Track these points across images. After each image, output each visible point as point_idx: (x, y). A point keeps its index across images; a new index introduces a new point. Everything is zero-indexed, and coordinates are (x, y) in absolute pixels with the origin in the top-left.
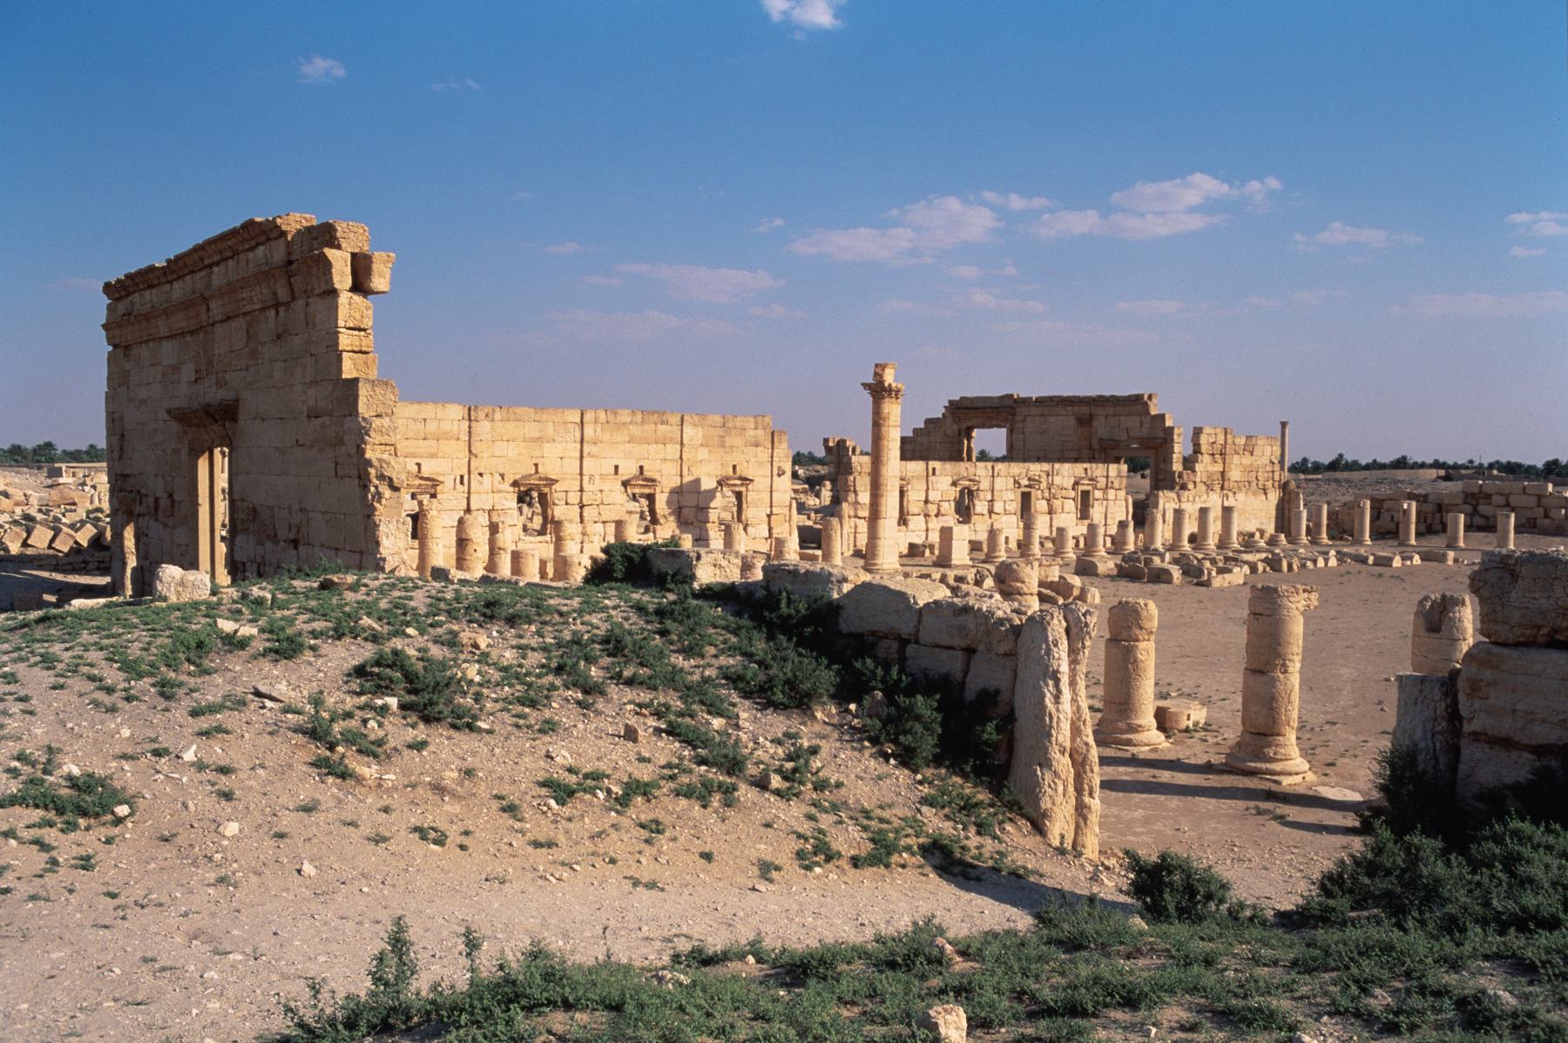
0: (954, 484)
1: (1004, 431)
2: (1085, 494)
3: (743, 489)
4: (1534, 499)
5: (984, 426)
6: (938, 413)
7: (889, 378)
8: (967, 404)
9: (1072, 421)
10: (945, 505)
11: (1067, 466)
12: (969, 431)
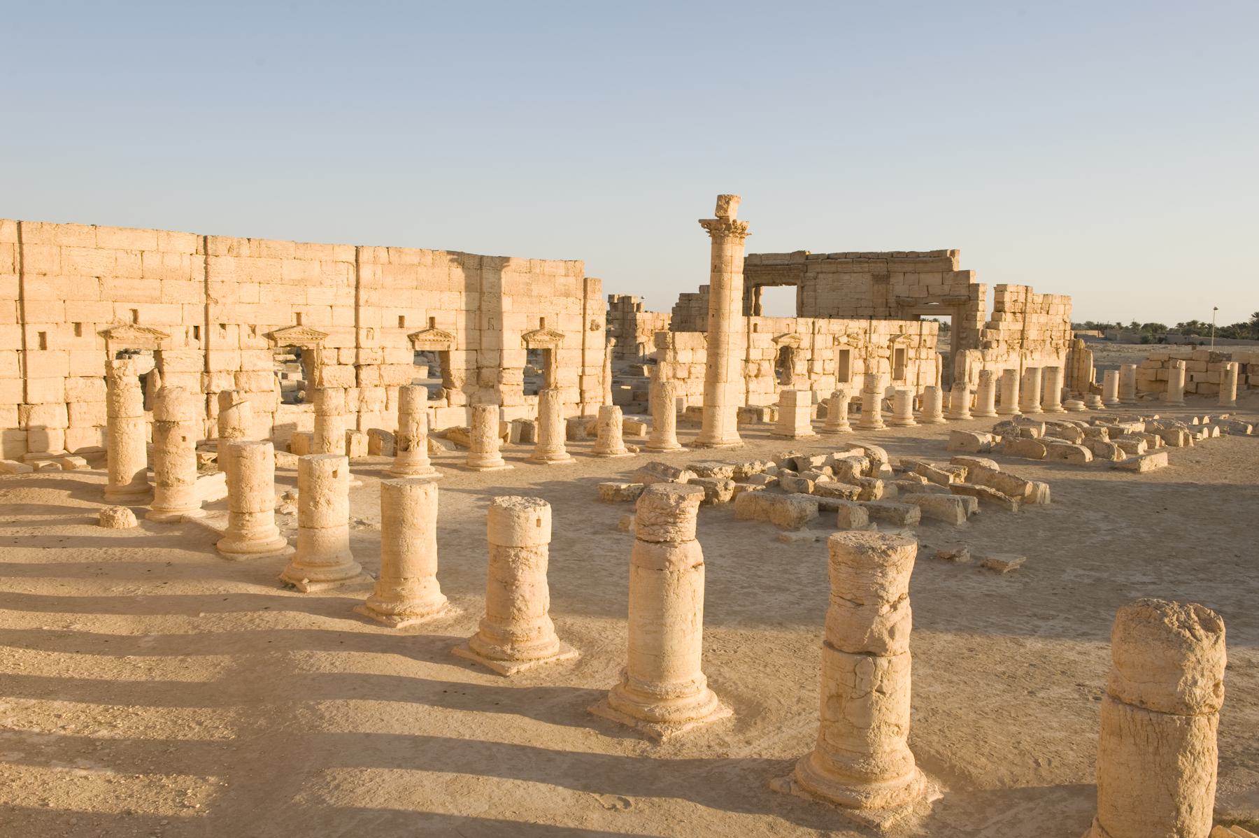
0: (775, 340)
2: (900, 352)
3: (551, 346)
7: (733, 213)
8: (757, 262)
9: (868, 277)
11: (883, 323)
12: (758, 286)
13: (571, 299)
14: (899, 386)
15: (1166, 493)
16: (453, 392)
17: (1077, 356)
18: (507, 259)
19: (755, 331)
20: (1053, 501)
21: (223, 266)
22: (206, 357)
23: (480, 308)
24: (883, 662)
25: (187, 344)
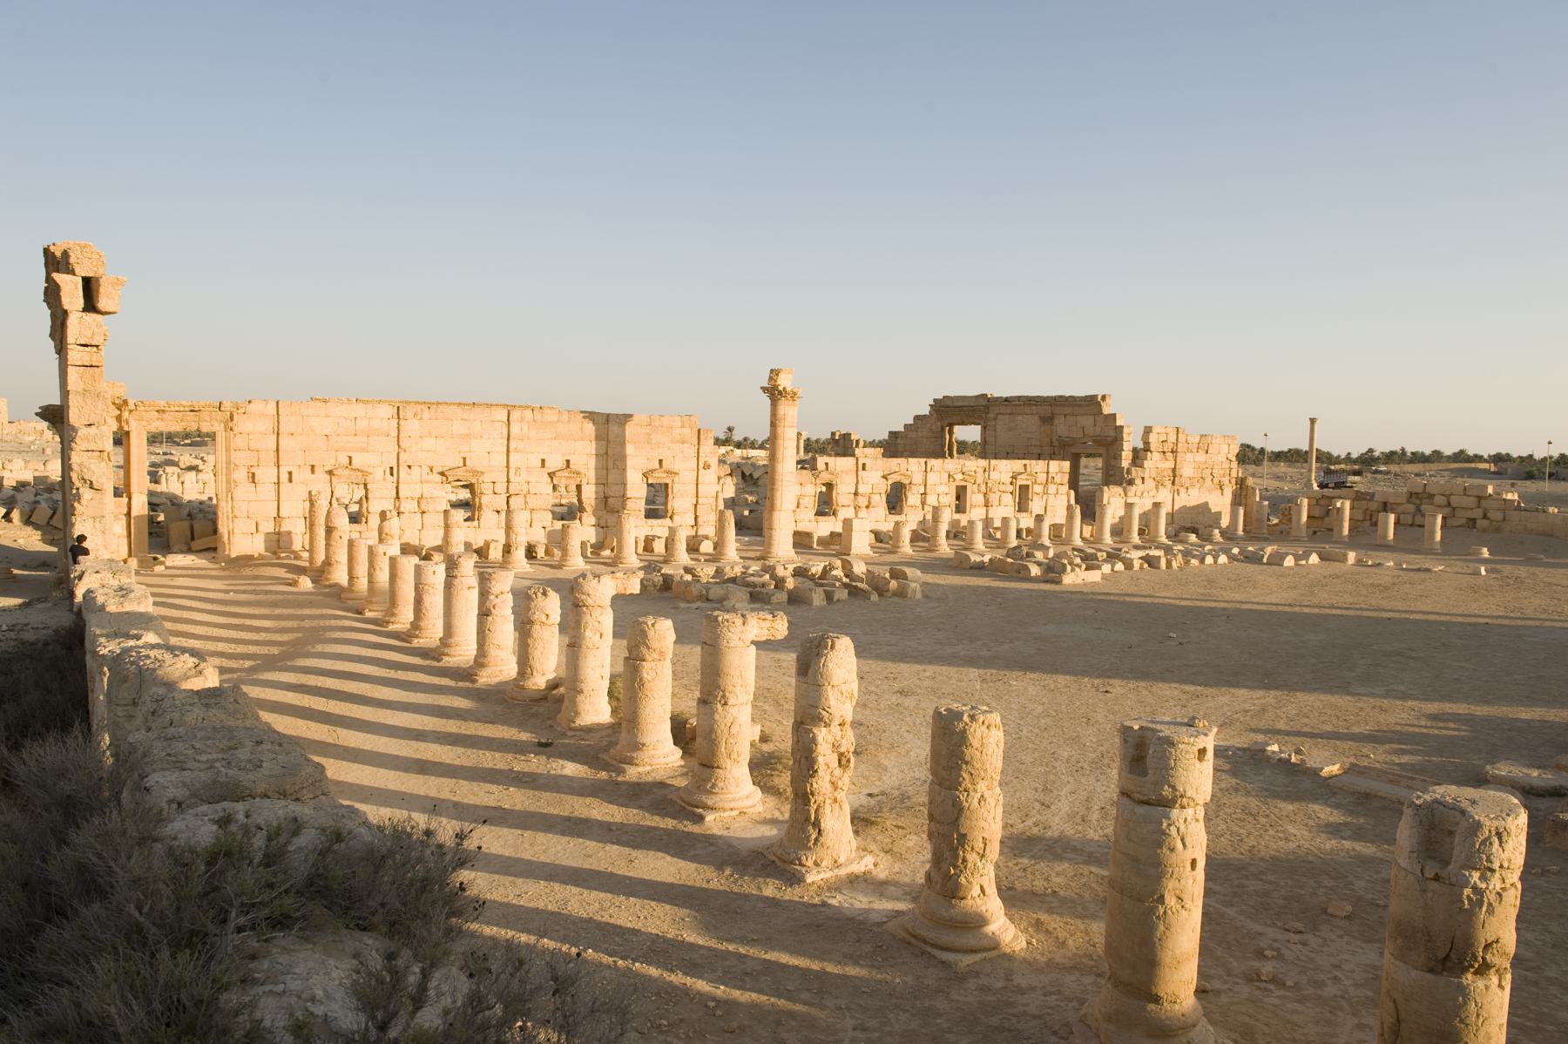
1: (979, 428)
2: (1024, 489)
4: (1474, 500)
6: (926, 411)
7: (784, 382)
8: (949, 403)
12: (951, 425)
14: (964, 520)
15: (1081, 597)
16: (585, 516)
20: (925, 596)
21: (411, 426)
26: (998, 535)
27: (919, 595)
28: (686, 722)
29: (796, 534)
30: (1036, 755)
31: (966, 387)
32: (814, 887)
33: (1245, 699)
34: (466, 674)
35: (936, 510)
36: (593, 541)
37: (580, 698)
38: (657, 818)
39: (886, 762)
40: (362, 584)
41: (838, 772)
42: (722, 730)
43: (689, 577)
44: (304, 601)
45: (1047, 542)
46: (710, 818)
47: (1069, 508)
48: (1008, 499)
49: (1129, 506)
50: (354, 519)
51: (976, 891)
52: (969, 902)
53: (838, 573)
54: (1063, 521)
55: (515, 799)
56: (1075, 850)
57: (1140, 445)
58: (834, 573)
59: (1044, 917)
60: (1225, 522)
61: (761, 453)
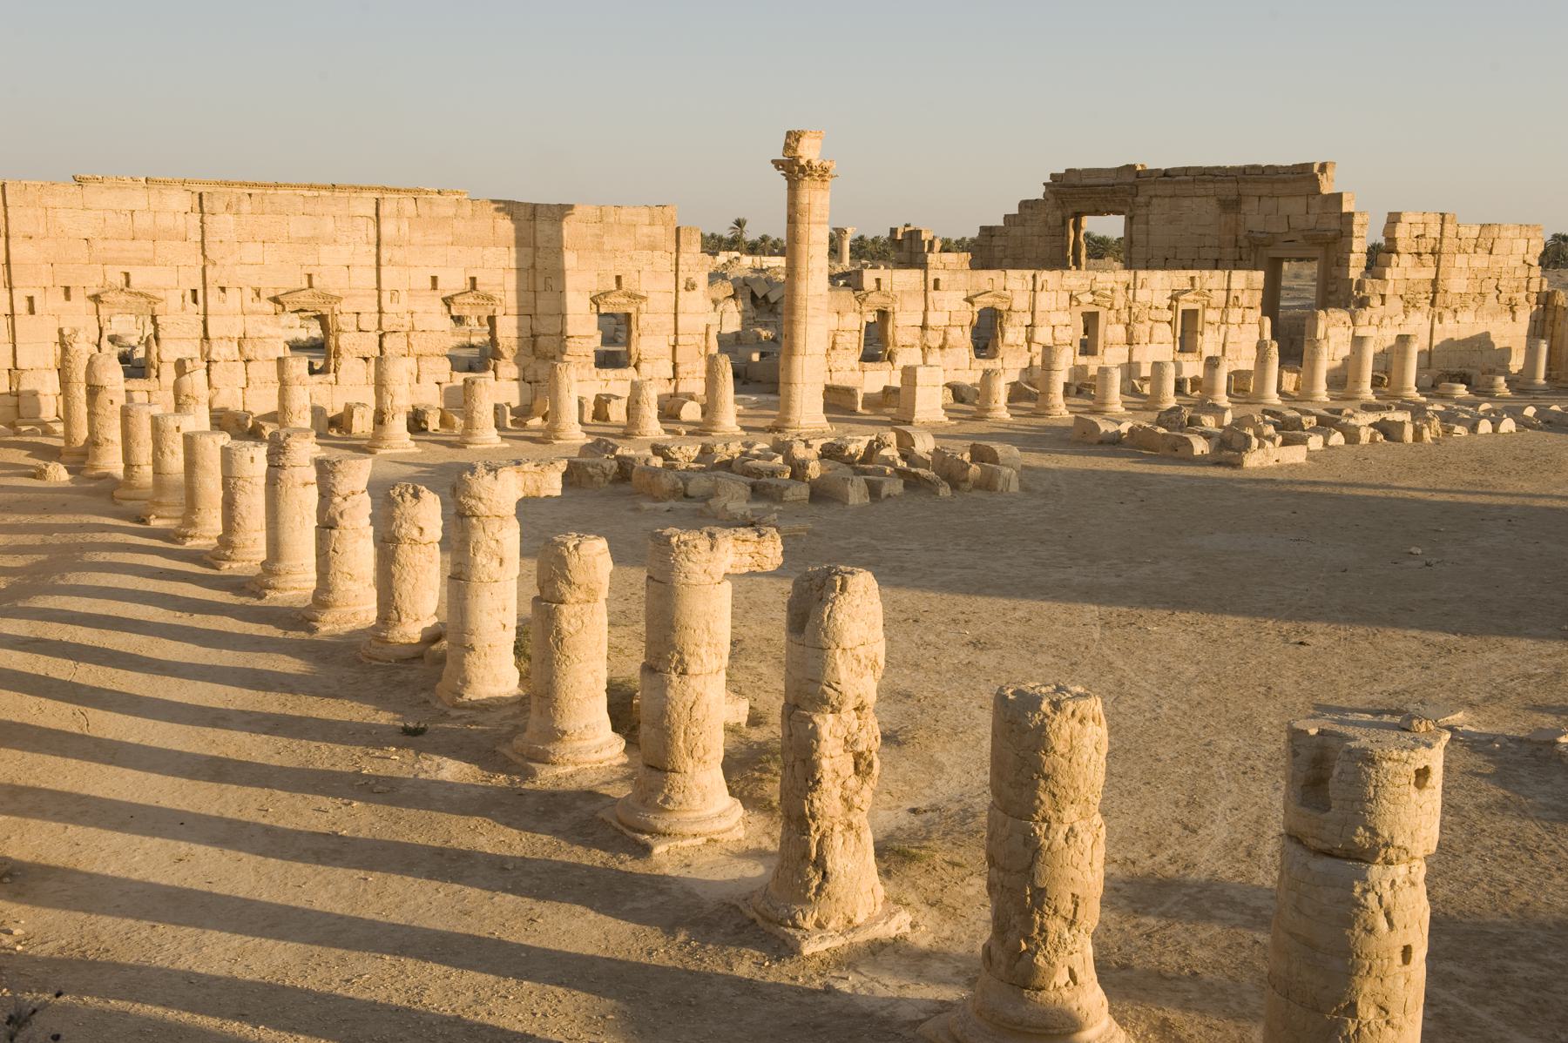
2: (1190, 317)
3: (631, 310)
5: (1097, 213)
6: (1038, 193)
7: (809, 151)
8: (1075, 180)
10: (955, 334)
11: (1159, 274)
12: (1078, 216)
13: (657, 253)
14: (1092, 365)
15: (1279, 493)
16: (502, 364)
17: (1550, 317)
18: (571, 207)
19: (936, 287)
20: (1025, 488)
21: (223, 224)
22: (205, 322)
23: (533, 266)
24: (335, 533)
25: (183, 309)
26: (1147, 390)
27: (1014, 487)
28: (632, 696)
29: (830, 390)
30: (1181, 746)
31: (1102, 153)
32: (815, 963)
33: (1526, 656)
34: (299, 619)
35: (1048, 351)
36: (516, 403)
37: (470, 659)
38: (579, 850)
39: (942, 757)
40: (146, 473)
41: (853, 782)
42: (679, 713)
43: (658, 462)
44: (56, 501)
45: (1223, 399)
46: (660, 849)
47: (1261, 346)
48: (1164, 333)
49: (1358, 342)
50: (135, 368)
51: (1062, 977)
52: (1051, 994)
53: (891, 452)
54: (1251, 366)
55: (359, 820)
56: (1231, 903)
57: (1382, 240)
58: (885, 452)
59: (1174, 1015)
60: (1516, 364)
61: (779, 262)
